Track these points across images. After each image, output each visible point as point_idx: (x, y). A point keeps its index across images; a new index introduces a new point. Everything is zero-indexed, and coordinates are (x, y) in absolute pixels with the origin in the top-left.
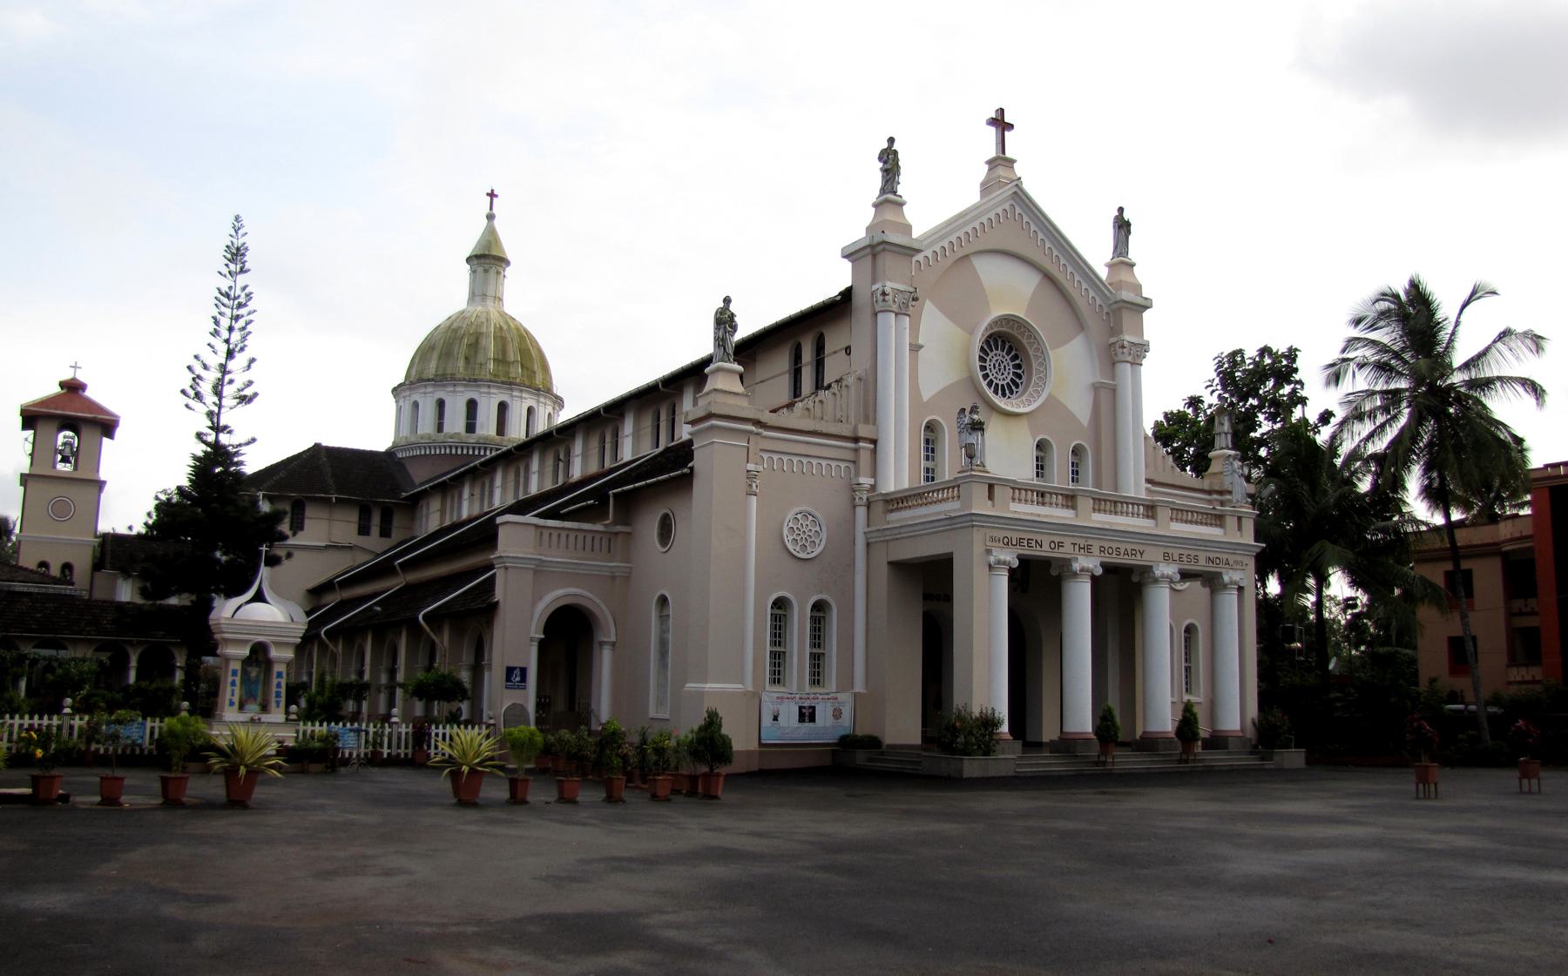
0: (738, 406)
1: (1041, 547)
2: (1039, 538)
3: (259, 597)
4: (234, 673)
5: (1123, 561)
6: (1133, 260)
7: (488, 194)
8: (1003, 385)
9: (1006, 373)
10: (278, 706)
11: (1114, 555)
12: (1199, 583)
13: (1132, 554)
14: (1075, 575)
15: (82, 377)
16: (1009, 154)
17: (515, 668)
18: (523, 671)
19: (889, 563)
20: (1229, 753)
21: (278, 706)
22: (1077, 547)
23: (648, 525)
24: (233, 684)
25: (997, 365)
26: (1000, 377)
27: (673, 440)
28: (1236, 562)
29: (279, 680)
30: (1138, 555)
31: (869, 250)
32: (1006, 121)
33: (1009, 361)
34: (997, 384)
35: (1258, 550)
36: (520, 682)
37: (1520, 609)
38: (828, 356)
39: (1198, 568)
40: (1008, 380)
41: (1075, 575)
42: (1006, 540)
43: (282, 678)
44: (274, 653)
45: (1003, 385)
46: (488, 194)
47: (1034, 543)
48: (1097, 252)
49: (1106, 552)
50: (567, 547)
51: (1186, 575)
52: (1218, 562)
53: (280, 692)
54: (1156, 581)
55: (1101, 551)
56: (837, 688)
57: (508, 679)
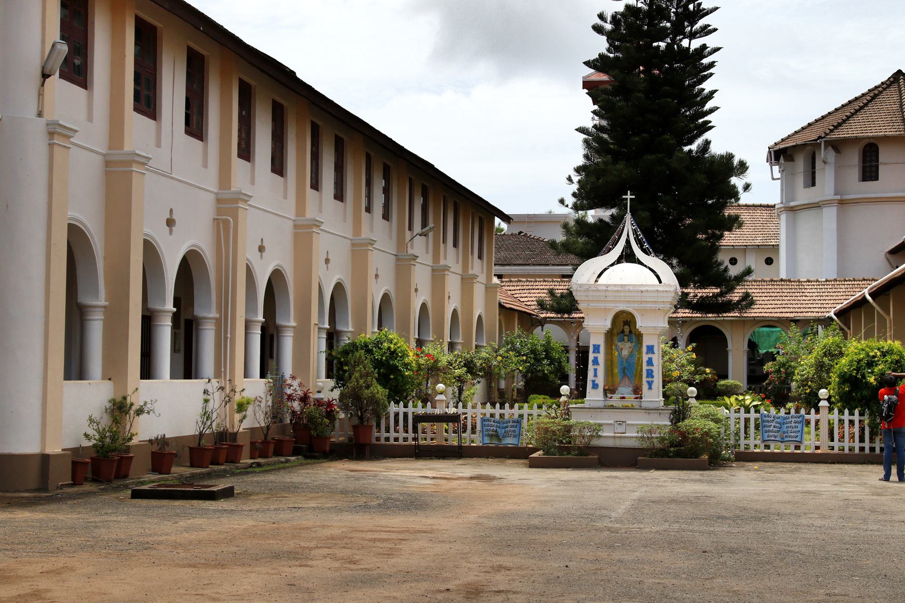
29: (650, 356)
43: (653, 353)
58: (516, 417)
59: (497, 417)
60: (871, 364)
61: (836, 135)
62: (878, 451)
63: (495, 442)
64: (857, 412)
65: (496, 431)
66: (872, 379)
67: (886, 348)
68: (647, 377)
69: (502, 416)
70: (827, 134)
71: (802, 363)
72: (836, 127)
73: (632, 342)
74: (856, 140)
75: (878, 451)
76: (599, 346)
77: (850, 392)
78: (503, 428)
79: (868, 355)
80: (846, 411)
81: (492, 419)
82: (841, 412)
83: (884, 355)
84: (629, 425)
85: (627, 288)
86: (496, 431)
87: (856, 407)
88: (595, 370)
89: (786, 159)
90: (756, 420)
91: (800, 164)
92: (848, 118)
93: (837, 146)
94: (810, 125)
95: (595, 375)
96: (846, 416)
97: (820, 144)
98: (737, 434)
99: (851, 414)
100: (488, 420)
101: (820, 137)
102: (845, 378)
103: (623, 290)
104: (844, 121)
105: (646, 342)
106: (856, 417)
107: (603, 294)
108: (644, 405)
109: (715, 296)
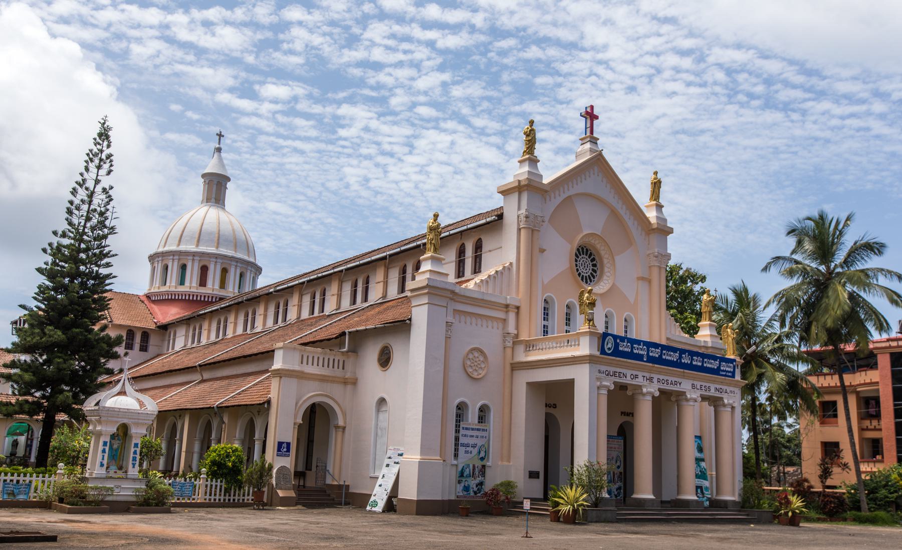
0: (443, 282)
3: (122, 393)
4: (105, 444)
5: (670, 388)
8: (586, 276)
9: (588, 269)
10: (134, 467)
11: (665, 384)
12: (707, 403)
14: (644, 395)
16: (595, 135)
17: (283, 443)
18: (288, 444)
19: (527, 383)
20: (729, 511)
21: (134, 467)
22: (645, 378)
23: (371, 353)
27: (323, 312)
28: (731, 391)
29: (136, 449)
31: (517, 189)
32: (595, 113)
33: (590, 262)
34: (583, 276)
35: (743, 385)
36: (286, 452)
37: (867, 427)
38: (485, 253)
40: (589, 274)
41: (644, 395)
42: (607, 372)
43: (138, 447)
44: (133, 430)
45: (586, 276)
47: (622, 374)
48: (641, 196)
50: (318, 365)
51: (704, 398)
53: (136, 458)
54: (687, 400)
57: (279, 450)
58: (27, 482)
59: (15, 482)
63: (12, 497)
64: (219, 480)
65: (13, 491)
67: (234, 448)
68: (133, 461)
69: (18, 481)
71: (836, 500)
73: (120, 440)
76: (107, 442)
78: (18, 489)
79: (226, 452)
81: (11, 483)
82: (212, 481)
83: (233, 452)
84: (123, 488)
85: (131, 411)
86: (13, 491)
87: (219, 478)
96: (214, 483)
100: (9, 484)
102: (214, 463)
106: (219, 484)
107: (117, 413)
108: (129, 476)
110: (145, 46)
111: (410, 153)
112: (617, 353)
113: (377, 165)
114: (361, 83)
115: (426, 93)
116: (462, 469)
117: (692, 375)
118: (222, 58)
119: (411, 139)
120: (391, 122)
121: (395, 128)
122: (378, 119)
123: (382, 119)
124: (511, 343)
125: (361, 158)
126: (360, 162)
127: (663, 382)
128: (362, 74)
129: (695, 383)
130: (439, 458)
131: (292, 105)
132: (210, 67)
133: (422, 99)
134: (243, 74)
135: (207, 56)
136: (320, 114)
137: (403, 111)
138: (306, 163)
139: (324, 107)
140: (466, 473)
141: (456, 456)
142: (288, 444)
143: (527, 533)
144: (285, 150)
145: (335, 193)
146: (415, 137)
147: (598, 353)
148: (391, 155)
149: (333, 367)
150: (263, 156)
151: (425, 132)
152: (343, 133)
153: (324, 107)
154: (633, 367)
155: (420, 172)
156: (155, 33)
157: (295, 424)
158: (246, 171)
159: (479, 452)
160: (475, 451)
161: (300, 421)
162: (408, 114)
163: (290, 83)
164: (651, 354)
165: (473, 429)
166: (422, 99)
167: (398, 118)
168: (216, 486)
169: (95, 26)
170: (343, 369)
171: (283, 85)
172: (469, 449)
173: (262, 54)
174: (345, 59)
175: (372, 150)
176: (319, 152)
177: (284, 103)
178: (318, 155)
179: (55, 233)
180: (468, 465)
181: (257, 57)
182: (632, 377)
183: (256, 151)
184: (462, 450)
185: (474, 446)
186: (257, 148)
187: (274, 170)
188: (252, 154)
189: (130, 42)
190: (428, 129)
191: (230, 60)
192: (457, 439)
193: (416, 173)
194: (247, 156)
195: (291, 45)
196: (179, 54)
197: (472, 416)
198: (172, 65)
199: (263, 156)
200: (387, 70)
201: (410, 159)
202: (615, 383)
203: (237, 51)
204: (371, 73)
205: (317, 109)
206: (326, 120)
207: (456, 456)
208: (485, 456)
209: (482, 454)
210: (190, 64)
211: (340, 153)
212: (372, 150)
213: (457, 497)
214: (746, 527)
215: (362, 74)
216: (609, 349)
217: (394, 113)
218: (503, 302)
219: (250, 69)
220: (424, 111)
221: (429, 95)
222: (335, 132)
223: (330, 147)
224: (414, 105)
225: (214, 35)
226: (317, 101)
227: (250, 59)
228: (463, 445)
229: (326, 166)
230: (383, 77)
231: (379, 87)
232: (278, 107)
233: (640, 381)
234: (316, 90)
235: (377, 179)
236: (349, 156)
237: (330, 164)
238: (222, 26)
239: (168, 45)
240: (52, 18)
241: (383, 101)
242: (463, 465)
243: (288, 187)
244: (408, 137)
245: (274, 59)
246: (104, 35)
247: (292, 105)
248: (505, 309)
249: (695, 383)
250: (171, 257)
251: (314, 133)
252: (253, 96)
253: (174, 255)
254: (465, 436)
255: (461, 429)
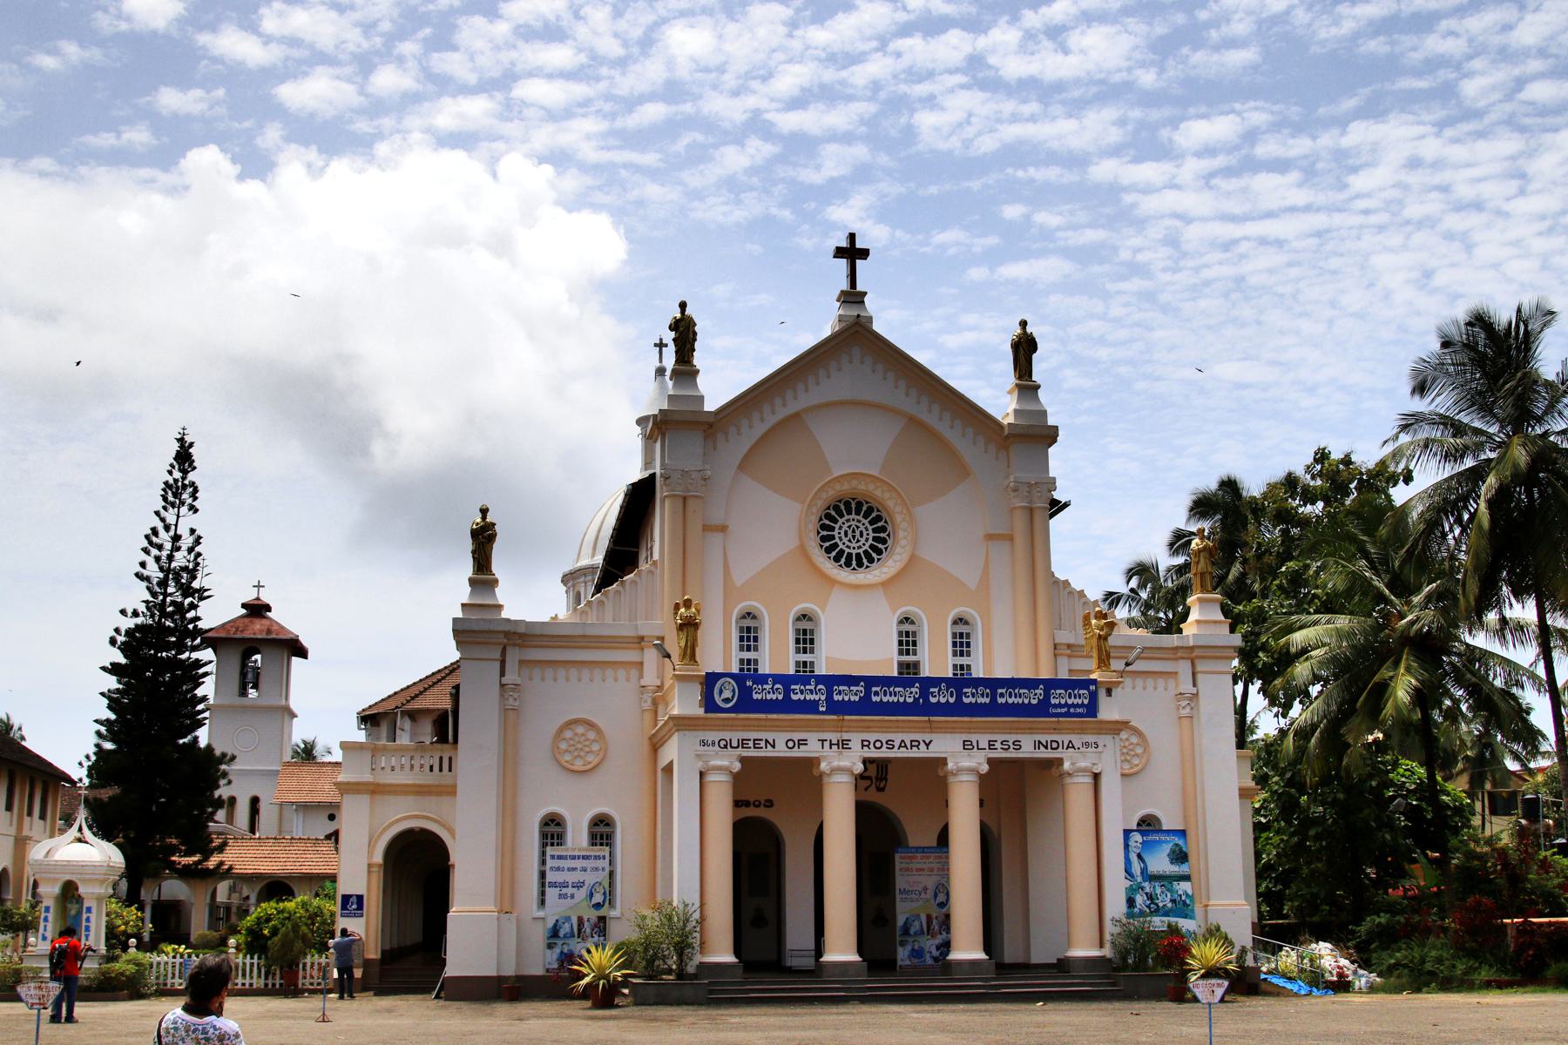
1: (774, 747)
2: (770, 736)
5: (906, 755)
6: (1038, 382)
7: (656, 345)
11: (884, 749)
13: (912, 746)
15: (266, 598)
16: (860, 288)
17: (351, 896)
20: (1074, 977)
22: (827, 744)
24: (46, 919)
25: (850, 533)
26: (854, 544)
28: (1087, 745)
30: (922, 746)
36: (357, 909)
39: (1020, 755)
42: (723, 743)
46: (656, 345)
47: (763, 744)
49: (871, 746)
52: (1055, 745)
55: (863, 746)
56: (1269, 900)
60: (268, 920)
61: (409, 707)
62: (278, 986)
64: (256, 957)
66: (266, 932)
70: (403, 704)
72: (413, 698)
74: (427, 711)
75: (278, 986)
77: (252, 941)
80: (248, 956)
82: (245, 956)
83: (279, 912)
88: (45, 926)
89: (372, 725)
90: (181, 964)
91: (384, 729)
92: (426, 689)
93: (413, 715)
94: (396, 693)
95: (45, 930)
96: (248, 960)
97: (396, 714)
98: (166, 975)
99: (252, 958)
101: (397, 707)
102: (250, 931)
103: (68, 865)
104: (421, 693)
105: (86, 904)
106: (255, 961)
109: (197, 863)
110: (943, 109)
111: (1522, 192)
112: (745, 703)
113: (1449, 236)
114: (1391, 66)
115: (1542, 53)
116: (555, 925)
117: (960, 725)
118: (1094, 89)
119: (1521, 162)
120: (1469, 134)
121: (1481, 145)
122: (1438, 135)
123: (1449, 133)
124: (649, 701)
125: (1409, 229)
126: (1408, 237)
127: (878, 744)
128: (1388, 48)
129: (974, 738)
130: (493, 908)
131: (1243, 152)
132: (1070, 116)
133: (1535, 65)
134: (1136, 114)
135: (1064, 95)
136: (1306, 157)
137: (1493, 104)
138: (1290, 265)
139: (1314, 138)
140: (565, 929)
141: (542, 902)
142: (360, 898)
143: (324, 1014)
144: (1244, 247)
145: (1360, 316)
146: (1531, 153)
147: (701, 712)
148: (1477, 206)
149: (441, 770)
150: (1197, 270)
151: (1548, 138)
152: (1359, 182)
153: (1314, 138)
154: (744, 726)
155: (1550, 231)
156: (960, 79)
157: (370, 866)
158: (1165, 309)
159: (591, 895)
160: (581, 894)
161: (378, 858)
162: (1508, 107)
163: (1237, 106)
164: (836, 698)
165: (573, 858)
166: (1535, 65)
167: (1487, 120)
168: (252, 965)
169: (850, 98)
170: (450, 771)
171: (1222, 113)
172: (569, 891)
173: (1171, 62)
174: (1347, 27)
175: (1432, 205)
176: (1319, 234)
177: (1231, 149)
178: (1314, 241)
179: (123, 612)
180: (918, 917)
181: (1162, 70)
182: (790, 744)
183: (1182, 263)
184: (551, 893)
185: (579, 885)
186: (1185, 255)
187: (1226, 295)
188: (1176, 270)
189: (913, 111)
190: (1556, 130)
191: (1104, 90)
192: (543, 875)
193: (1540, 234)
194: (1167, 277)
195: (1224, 29)
196: (1009, 106)
197: (577, 835)
198: (996, 130)
199: (1197, 270)
200: (1445, 24)
201: (1522, 206)
202: (743, 760)
203: (1120, 70)
204: (1407, 40)
205: (1301, 146)
206: (1320, 166)
207: (542, 902)
208: (604, 901)
209: (941, 898)
210: (1033, 119)
211: (1361, 227)
212: (1432, 205)
213: (548, 970)
214: (1032, 1007)
215: (1388, 48)
216: (727, 700)
217: (1477, 114)
218: (632, 633)
219: (1150, 99)
220: (1541, 91)
221: (1550, 56)
222: (1344, 186)
223: (1338, 219)
224: (1520, 83)
225: (1066, 51)
226: (1298, 129)
227: (1147, 79)
228: (553, 885)
229: (1334, 263)
230: (1434, 44)
231: (1434, 64)
232: (1220, 161)
233: (812, 749)
234: (1295, 108)
235: (1453, 265)
236: (1381, 228)
237: (1342, 255)
238: (1085, 27)
239: (988, 95)
240: (775, 106)
241: (1447, 92)
242: (908, 915)
243: (1259, 323)
244: (1513, 158)
245: (1194, 67)
246: (871, 108)
247: (1243, 152)
248: (637, 645)
249: (974, 738)
250: (582, 579)
251: (1301, 197)
252: (1165, 153)
253: (585, 575)
254: (558, 869)
255: (548, 858)
